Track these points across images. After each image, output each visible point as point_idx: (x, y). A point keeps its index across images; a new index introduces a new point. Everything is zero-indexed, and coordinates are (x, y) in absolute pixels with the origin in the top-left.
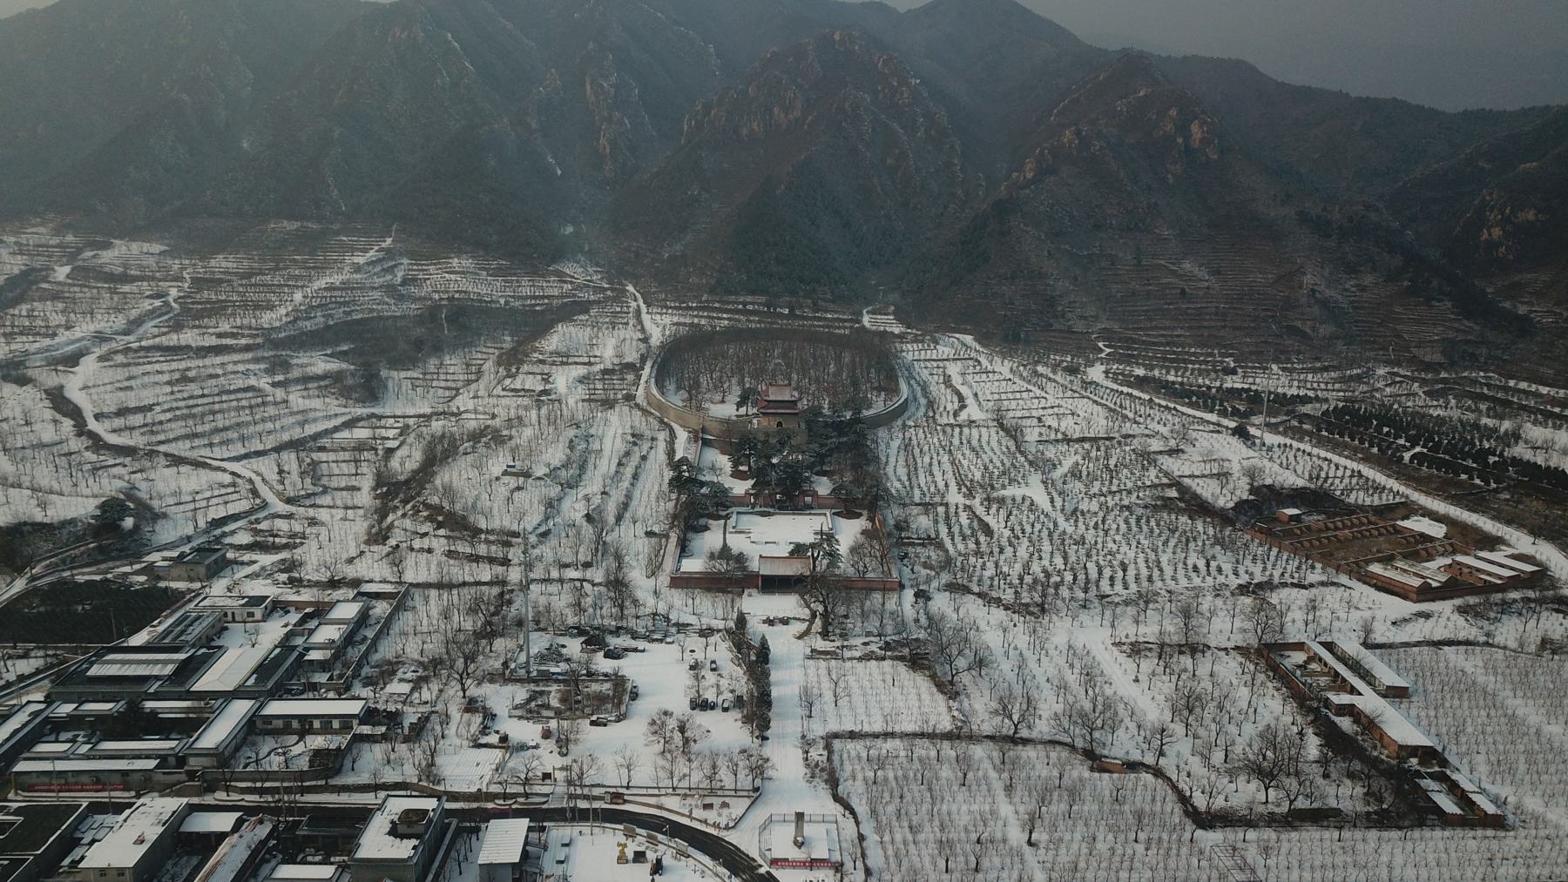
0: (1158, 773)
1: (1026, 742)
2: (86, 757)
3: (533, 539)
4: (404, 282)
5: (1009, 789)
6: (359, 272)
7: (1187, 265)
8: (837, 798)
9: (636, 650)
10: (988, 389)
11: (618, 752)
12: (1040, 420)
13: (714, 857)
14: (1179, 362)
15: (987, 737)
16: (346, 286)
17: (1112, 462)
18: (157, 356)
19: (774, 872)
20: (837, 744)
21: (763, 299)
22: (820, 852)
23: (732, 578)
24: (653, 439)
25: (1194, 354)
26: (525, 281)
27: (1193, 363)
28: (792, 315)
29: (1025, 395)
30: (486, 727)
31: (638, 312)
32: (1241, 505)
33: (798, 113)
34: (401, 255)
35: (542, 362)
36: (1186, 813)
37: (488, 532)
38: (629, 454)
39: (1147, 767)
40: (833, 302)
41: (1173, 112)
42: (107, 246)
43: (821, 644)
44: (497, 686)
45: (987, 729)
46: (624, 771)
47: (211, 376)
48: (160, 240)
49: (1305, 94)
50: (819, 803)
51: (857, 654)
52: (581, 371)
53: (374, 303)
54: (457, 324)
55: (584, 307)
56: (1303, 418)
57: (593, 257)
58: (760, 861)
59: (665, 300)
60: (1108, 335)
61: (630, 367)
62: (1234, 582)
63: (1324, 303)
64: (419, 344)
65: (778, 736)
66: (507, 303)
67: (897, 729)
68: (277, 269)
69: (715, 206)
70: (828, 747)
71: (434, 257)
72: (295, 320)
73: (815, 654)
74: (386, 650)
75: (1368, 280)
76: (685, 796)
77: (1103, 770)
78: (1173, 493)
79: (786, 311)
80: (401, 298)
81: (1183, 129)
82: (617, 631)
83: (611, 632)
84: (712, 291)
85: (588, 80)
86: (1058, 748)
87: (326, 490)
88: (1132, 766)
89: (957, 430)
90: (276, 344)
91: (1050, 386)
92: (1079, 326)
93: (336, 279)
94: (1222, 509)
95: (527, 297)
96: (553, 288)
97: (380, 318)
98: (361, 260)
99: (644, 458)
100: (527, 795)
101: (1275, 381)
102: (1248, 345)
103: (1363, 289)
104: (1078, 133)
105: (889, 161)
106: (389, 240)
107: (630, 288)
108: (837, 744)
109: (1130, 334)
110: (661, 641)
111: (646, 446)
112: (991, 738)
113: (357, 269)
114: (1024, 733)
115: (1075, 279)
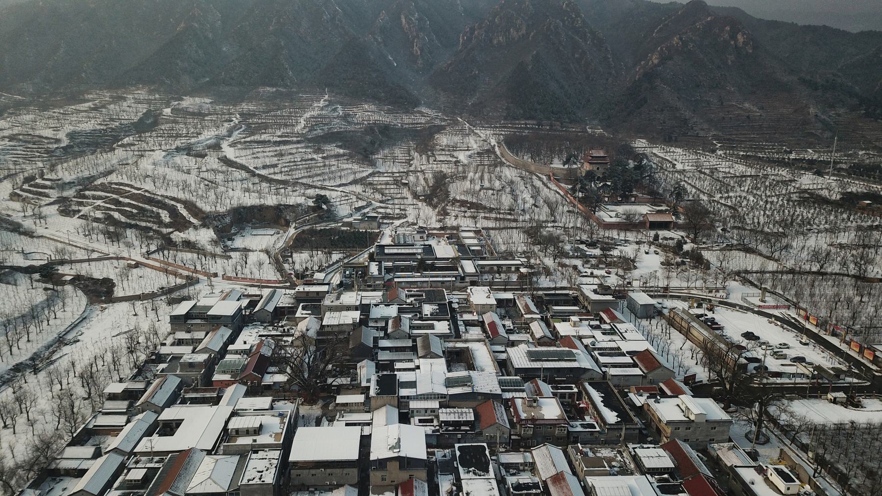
2: (419, 277)
7: (747, 105)
14: (762, 149)
18: (256, 145)
21: (535, 122)
28: (550, 130)
33: (524, 31)
40: (571, 123)
41: (728, 28)
42: (182, 100)
47: (291, 154)
48: (207, 96)
60: (716, 137)
63: (823, 122)
71: (355, 105)
75: (842, 111)
81: (733, 37)
84: (505, 119)
85: (402, 16)
92: (702, 134)
103: (839, 115)
104: (681, 39)
105: (577, 56)
106: (327, 96)
109: (728, 137)
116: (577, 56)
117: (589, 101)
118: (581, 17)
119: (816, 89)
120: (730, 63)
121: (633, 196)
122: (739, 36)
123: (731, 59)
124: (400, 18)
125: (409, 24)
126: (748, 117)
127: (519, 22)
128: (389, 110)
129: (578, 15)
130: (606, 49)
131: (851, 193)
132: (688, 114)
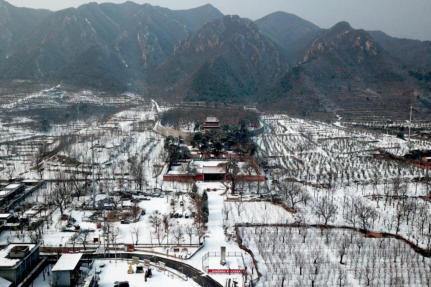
0: (398, 237)
1: (332, 227)
3: (103, 166)
4: (64, 98)
5: (327, 242)
6: (46, 95)
8: (241, 247)
9: (146, 199)
10: (296, 126)
11: (136, 233)
12: (318, 133)
13: (180, 271)
14: (370, 120)
15: (312, 226)
16: (39, 98)
17: (350, 144)
19: (210, 275)
20: (240, 228)
22: (234, 266)
23: (193, 177)
24: (159, 140)
25: (375, 118)
26: (111, 99)
27: (375, 120)
29: (311, 127)
30: (70, 224)
31: (155, 107)
32: (407, 156)
33: (217, 43)
34: (63, 90)
35: (115, 120)
36: (416, 251)
37: (84, 163)
38: (149, 146)
39: (392, 235)
40: (232, 103)
41: (359, 38)
43: (231, 196)
44: (79, 211)
45: (313, 222)
46: (135, 236)
49: (404, 41)
50: (233, 247)
51: (248, 200)
52: (131, 122)
53: (52, 103)
54: (85, 111)
55: (135, 106)
56: (423, 135)
57: (138, 92)
58: (203, 271)
59: (167, 104)
60: (339, 113)
61: (151, 121)
62: (411, 177)
63: (423, 101)
64: (67, 116)
65: (212, 219)
66: (103, 105)
67: (269, 223)
68: (13, 93)
69: (186, 75)
70: (236, 229)
72: (17, 107)
73: (228, 199)
74: (30, 200)
76: (165, 247)
77: (371, 236)
78: (378, 153)
79: (214, 107)
80: (62, 102)
81: (363, 44)
82: (138, 193)
83: (135, 194)
84: (185, 100)
86: (347, 229)
87: (17, 155)
88: (385, 235)
89: (285, 137)
90: (8, 114)
91: (320, 126)
92: (329, 110)
93: (36, 96)
94: (400, 157)
95: (112, 104)
96: (122, 101)
97: (53, 108)
98: (47, 91)
99: (155, 145)
100: (85, 248)
101: (408, 124)
102: (396, 114)
104: (324, 45)
105: (252, 58)
107: (153, 101)
108: (240, 228)
110: (158, 196)
111: (155, 142)
112: (315, 226)
113: (45, 93)
114: (329, 223)
115: (326, 94)
116: (252, 58)
117: (257, 89)
118: (259, 33)
119: (421, 79)
120: (360, 62)
121: (222, 153)
122: (367, 44)
123: (360, 59)
124: (137, 36)
125: (141, 39)
126: (368, 99)
127: (214, 36)
128: (102, 94)
129: (257, 31)
130: (276, 54)
131: (417, 151)
132: (320, 96)
